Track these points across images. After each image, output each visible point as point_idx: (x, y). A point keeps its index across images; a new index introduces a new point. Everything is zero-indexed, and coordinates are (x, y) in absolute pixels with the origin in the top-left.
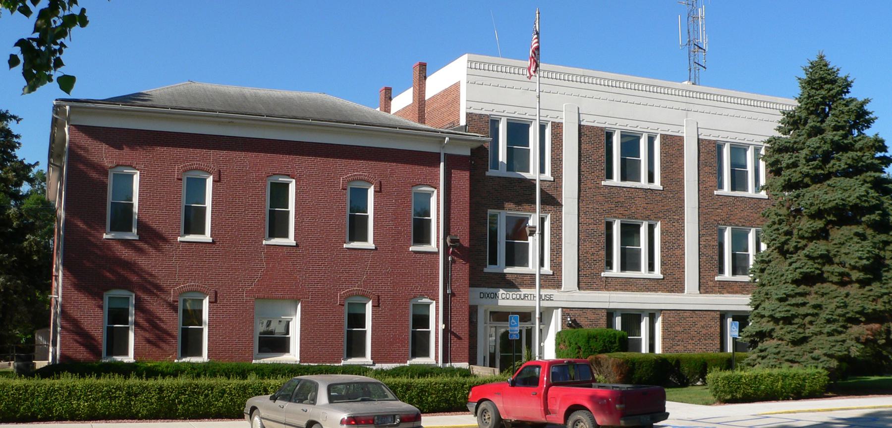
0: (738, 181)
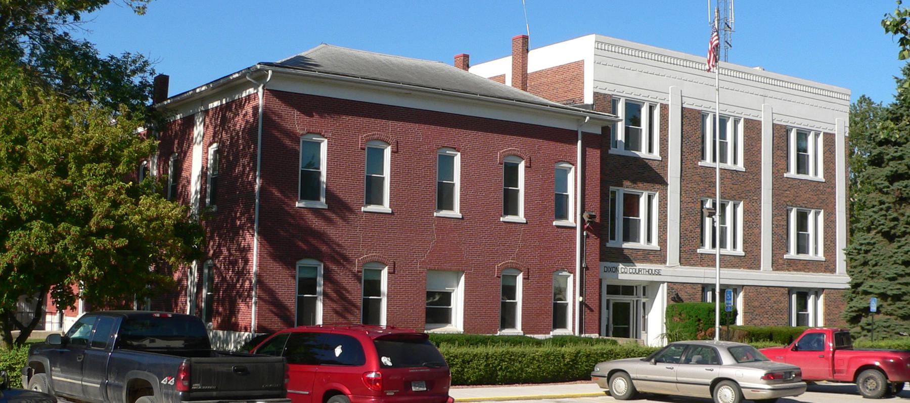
0: (802, 166)
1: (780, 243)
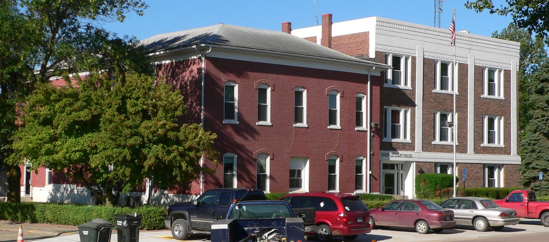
0: (491, 91)
1: (479, 137)
